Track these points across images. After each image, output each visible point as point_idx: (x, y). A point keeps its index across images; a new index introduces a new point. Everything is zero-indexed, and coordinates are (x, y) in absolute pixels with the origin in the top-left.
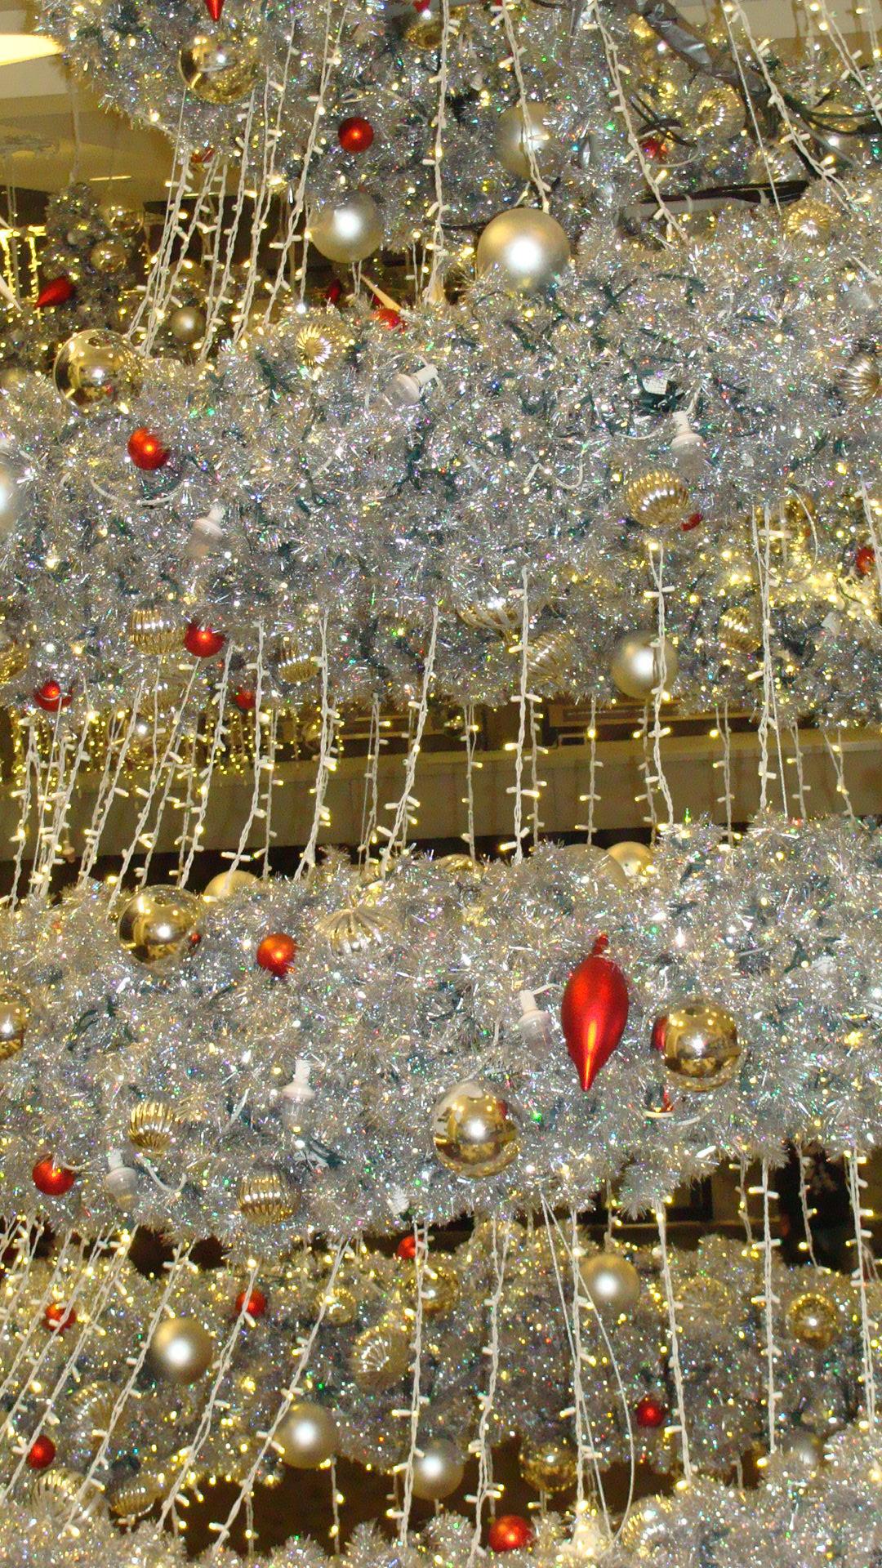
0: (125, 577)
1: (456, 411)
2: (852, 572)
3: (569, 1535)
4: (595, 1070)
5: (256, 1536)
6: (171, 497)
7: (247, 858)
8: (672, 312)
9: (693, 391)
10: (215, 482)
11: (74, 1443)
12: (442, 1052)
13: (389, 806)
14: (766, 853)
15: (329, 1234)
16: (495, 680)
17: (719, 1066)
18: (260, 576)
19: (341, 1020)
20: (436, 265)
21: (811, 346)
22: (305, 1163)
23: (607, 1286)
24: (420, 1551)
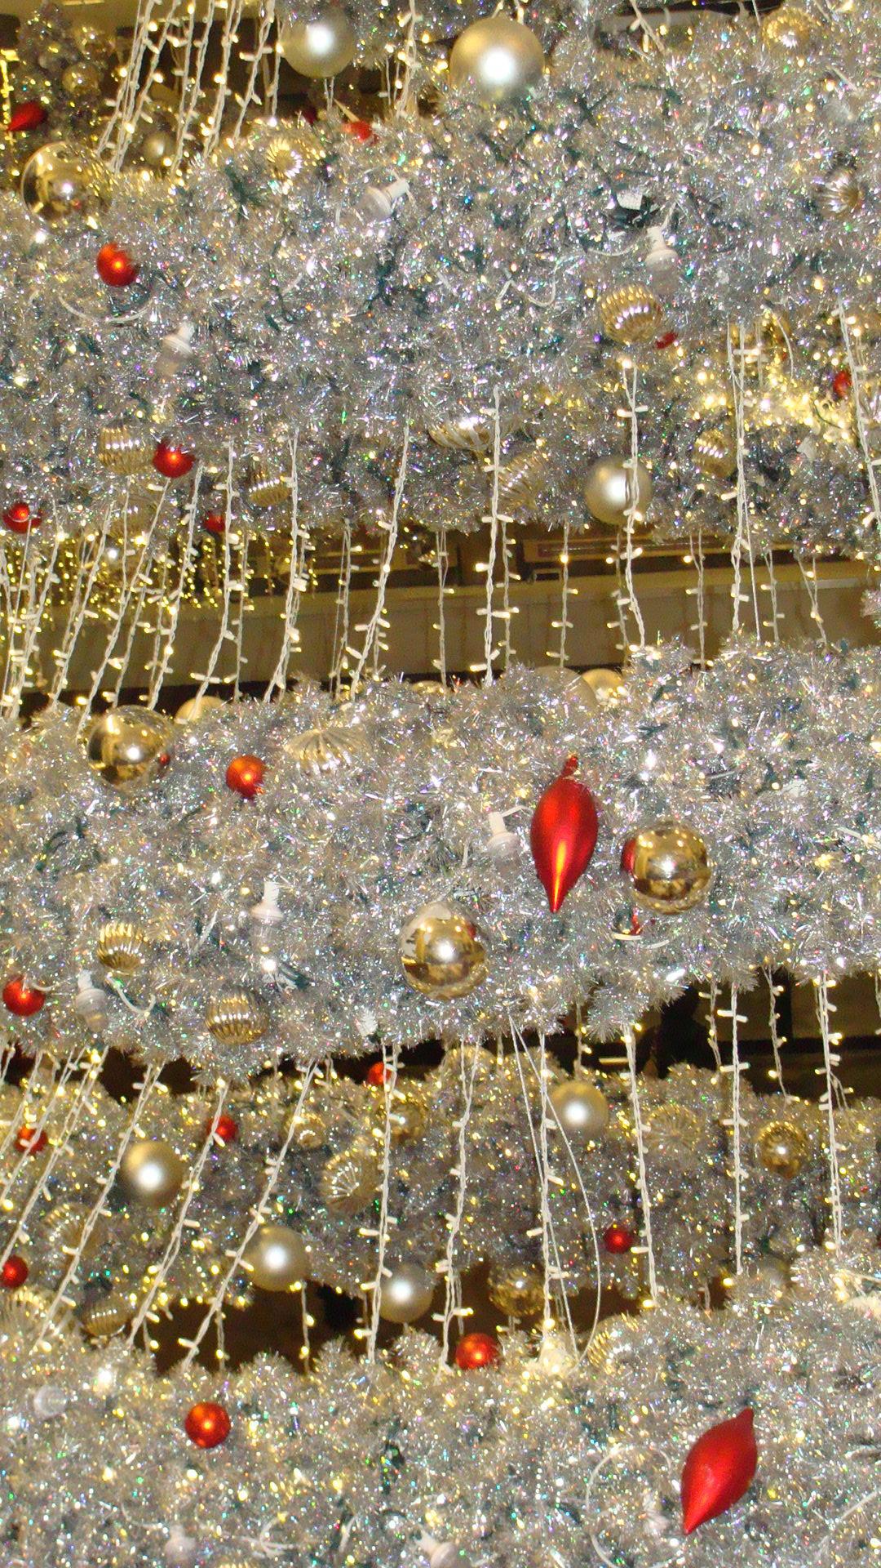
0: (93, 395)
1: (429, 227)
2: (829, 396)
3: (535, 1354)
4: (564, 892)
5: (227, 1357)
6: (141, 314)
7: (216, 680)
8: (647, 125)
9: (668, 206)
10: (185, 297)
11: (46, 1264)
12: (411, 874)
13: (359, 628)
14: (737, 676)
15: (297, 1056)
16: (468, 505)
17: (688, 887)
18: (229, 394)
19: (310, 841)
20: (408, 77)
21: (788, 159)
22: (275, 986)
23: (577, 1114)
24: (387, 1369)
